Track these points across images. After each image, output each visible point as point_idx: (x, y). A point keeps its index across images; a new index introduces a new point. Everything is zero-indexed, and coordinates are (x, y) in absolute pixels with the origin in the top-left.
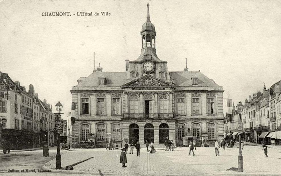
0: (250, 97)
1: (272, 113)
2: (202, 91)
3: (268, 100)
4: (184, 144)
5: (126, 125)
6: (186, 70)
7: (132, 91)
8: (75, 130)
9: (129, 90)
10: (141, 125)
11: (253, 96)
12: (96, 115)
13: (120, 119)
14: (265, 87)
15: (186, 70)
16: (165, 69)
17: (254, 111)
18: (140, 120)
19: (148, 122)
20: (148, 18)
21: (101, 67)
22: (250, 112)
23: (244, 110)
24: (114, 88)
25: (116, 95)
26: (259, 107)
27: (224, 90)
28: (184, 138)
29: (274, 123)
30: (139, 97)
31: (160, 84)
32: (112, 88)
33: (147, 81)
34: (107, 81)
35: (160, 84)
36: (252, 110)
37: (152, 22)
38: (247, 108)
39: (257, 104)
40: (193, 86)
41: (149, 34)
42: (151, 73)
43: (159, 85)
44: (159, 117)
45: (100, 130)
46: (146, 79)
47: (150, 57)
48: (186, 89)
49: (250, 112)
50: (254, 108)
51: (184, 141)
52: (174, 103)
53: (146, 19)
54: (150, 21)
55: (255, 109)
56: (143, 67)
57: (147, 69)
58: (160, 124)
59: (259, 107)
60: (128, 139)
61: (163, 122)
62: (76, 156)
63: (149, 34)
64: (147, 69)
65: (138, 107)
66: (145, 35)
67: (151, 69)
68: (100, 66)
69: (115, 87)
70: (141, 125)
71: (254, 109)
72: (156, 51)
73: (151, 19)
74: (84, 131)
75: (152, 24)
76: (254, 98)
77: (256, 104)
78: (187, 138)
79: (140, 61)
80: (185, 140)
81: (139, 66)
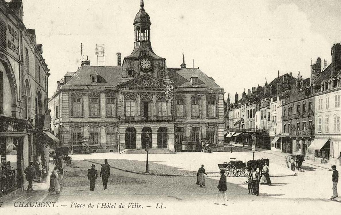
0: (249, 91)
1: (273, 117)
2: (202, 93)
3: (269, 100)
4: (183, 149)
5: (122, 128)
6: (183, 66)
7: (129, 91)
8: (66, 132)
9: (126, 90)
10: (139, 127)
11: (253, 90)
12: (88, 117)
13: (115, 121)
14: (266, 82)
15: (183, 66)
16: (163, 67)
17: (254, 109)
18: (137, 122)
19: (146, 125)
20: (142, 6)
21: (89, 60)
22: (248, 111)
23: (242, 107)
24: (109, 87)
25: (111, 96)
26: (260, 106)
27: (225, 92)
28: (183, 143)
29: (274, 127)
30: (136, 98)
31: (159, 84)
32: (107, 87)
33: (145, 80)
34: (100, 79)
35: (159, 84)
36: (251, 109)
37: (147, 11)
38: (245, 105)
39: (257, 103)
40: (193, 86)
41: (143, 23)
42: (149, 71)
43: (158, 86)
44: (159, 119)
45: (93, 134)
46: (144, 78)
47: (144, 50)
48: (185, 90)
49: (248, 111)
50: (253, 107)
51: (184, 146)
52: (173, 105)
53: (140, 8)
54: (144, 10)
55: (255, 108)
56: (141, 64)
57: (144, 67)
58: (158, 128)
59: (260, 106)
60: (125, 143)
61: (162, 125)
62: (307, 176)
63: (143, 23)
64: (144, 67)
65: (134, 108)
66: (140, 27)
67: (149, 67)
68: (87, 59)
69: (110, 86)
70: (139, 127)
71: (252, 108)
72: (150, 44)
73: (145, 8)
74: (76, 134)
75: (146, 13)
76: (253, 93)
77: (256, 101)
78: (187, 143)
79: (137, 56)
80: (185, 145)
81: (136, 62)
